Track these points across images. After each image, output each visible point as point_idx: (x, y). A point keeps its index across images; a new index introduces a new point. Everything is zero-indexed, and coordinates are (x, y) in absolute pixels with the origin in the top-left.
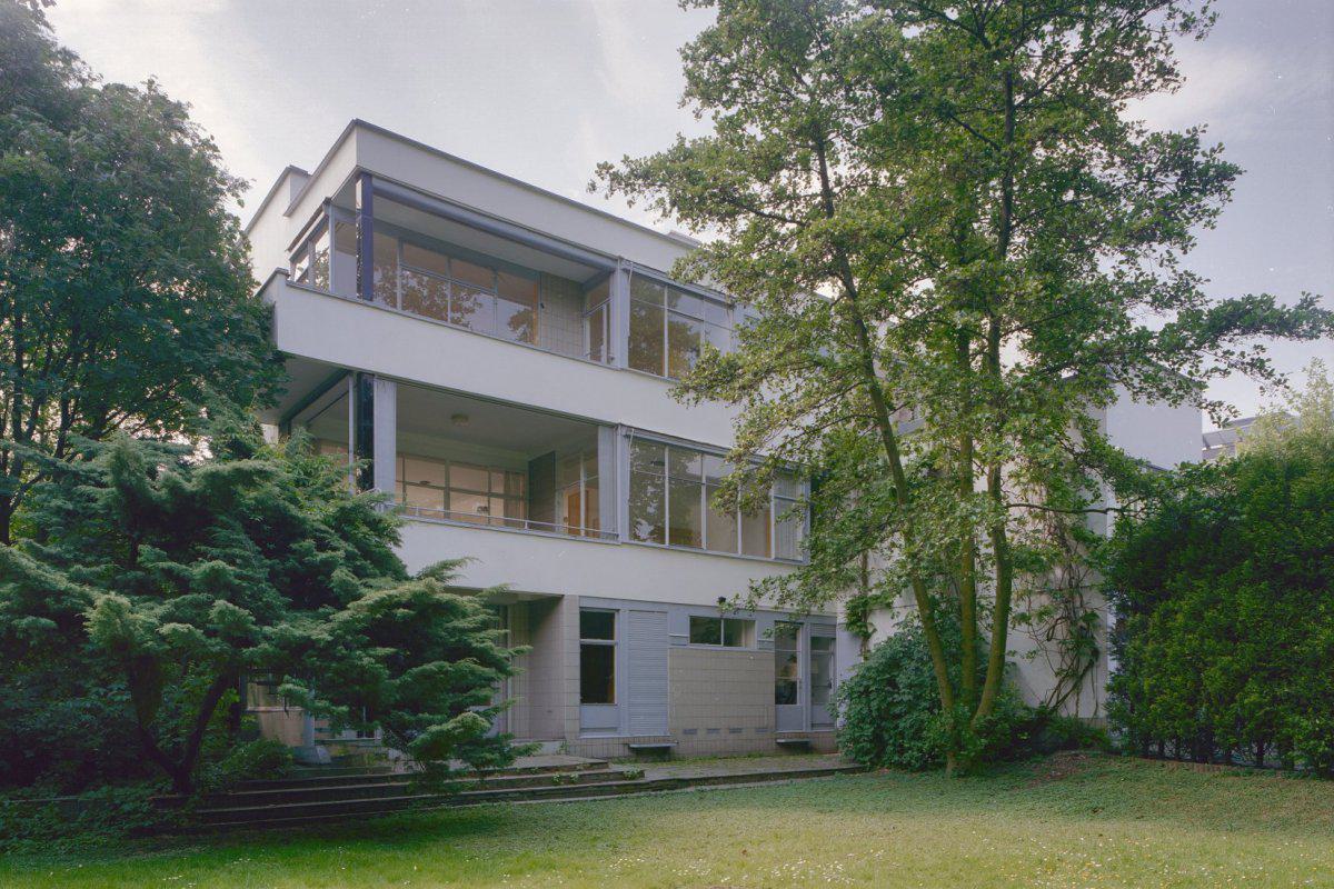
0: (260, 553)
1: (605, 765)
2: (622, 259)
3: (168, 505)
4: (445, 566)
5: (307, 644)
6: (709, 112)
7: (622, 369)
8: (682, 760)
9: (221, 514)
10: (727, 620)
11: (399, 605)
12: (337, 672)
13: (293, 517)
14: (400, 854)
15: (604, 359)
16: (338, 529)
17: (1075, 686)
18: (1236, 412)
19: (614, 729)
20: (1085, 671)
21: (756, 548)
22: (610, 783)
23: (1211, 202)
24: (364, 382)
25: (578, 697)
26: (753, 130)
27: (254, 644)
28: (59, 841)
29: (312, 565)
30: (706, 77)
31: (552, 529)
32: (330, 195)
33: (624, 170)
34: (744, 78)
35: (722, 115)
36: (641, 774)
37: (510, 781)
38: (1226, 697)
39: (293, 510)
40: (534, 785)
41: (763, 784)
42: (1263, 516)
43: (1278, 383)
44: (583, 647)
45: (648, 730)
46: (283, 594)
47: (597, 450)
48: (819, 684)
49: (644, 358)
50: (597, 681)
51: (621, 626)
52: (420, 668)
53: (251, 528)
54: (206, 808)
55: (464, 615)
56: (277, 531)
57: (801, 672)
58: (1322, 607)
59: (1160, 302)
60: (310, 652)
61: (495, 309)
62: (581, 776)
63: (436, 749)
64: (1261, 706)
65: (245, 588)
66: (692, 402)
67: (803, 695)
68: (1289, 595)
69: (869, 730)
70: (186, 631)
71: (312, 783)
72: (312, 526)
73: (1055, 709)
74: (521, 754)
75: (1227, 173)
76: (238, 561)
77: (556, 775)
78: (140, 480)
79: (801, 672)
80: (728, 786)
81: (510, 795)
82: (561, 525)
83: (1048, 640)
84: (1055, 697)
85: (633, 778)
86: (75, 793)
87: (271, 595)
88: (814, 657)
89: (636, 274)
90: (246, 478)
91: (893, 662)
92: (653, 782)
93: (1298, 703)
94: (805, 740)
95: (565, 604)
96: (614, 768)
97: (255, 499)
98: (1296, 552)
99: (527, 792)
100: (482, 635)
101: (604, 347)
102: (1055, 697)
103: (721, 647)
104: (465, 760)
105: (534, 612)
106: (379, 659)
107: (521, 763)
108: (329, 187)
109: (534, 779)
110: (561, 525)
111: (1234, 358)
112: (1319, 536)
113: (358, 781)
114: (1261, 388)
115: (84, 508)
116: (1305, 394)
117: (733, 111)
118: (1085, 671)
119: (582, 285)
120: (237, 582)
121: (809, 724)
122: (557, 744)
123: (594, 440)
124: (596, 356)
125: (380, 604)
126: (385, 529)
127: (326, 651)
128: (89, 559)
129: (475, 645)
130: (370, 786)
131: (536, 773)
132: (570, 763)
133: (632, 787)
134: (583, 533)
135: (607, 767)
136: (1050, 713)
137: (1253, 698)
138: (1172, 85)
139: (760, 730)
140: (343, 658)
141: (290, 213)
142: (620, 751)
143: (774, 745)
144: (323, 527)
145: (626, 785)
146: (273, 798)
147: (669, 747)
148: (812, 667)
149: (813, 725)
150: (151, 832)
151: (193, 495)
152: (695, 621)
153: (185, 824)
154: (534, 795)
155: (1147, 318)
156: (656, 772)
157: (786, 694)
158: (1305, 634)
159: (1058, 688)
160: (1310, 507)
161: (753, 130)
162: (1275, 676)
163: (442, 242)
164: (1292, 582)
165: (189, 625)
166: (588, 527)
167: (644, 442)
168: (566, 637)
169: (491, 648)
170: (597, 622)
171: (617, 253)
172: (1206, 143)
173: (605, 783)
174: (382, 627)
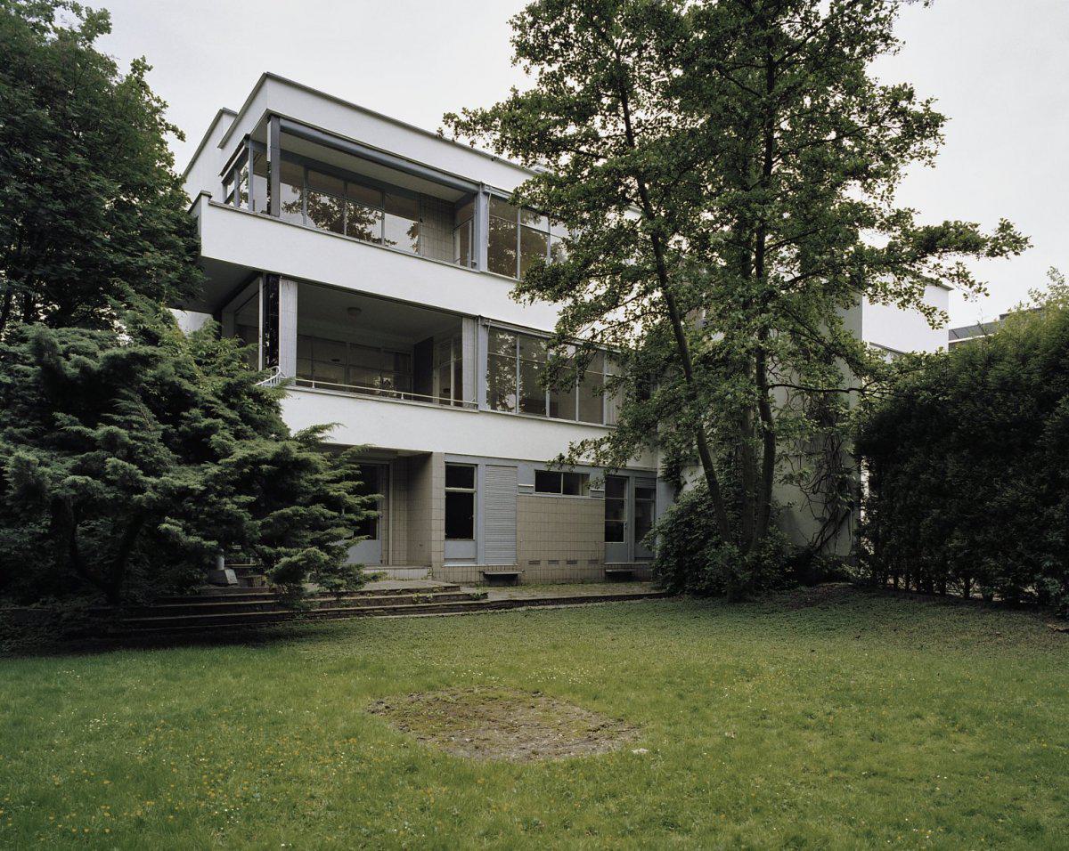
0: (155, 419)
1: (457, 588)
3: (79, 382)
4: (316, 429)
5: (185, 492)
6: (536, 69)
8: (527, 584)
9: (123, 388)
11: (266, 462)
12: (209, 515)
13: (188, 391)
15: (469, 264)
16: (224, 400)
18: (947, 317)
19: (473, 560)
21: (592, 415)
22: (458, 603)
26: (571, 82)
27: (142, 491)
28: (7, 642)
29: (198, 430)
30: (532, 42)
31: (430, 401)
33: (464, 119)
34: (563, 41)
35: (546, 71)
36: (485, 595)
37: (377, 600)
39: (187, 385)
42: (965, 396)
43: (979, 291)
44: (448, 494)
45: (500, 562)
46: (175, 451)
47: (461, 336)
48: (642, 525)
49: (499, 264)
50: (460, 522)
51: (480, 477)
52: (280, 512)
53: (147, 399)
54: (132, 617)
57: (628, 517)
59: (887, 226)
60: (188, 498)
61: (396, 227)
63: (292, 574)
65: (140, 447)
66: (528, 302)
67: (628, 533)
70: (84, 482)
72: (203, 398)
73: (820, 548)
75: (936, 120)
77: (415, 595)
78: (58, 362)
79: (628, 517)
81: (376, 611)
83: (814, 493)
84: (819, 540)
87: (163, 452)
88: (638, 504)
90: (146, 361)
91: (693, 506)
92: (492, 602)
94: (631, 570)
95: (434, 459)
96: (465, 590)
97: (154, 376)
99: (390, 609)
100: (339, 486)
101: (469, 254)
102: (819, 540)
103: (560, 495)
104: (321, 585)
106: (241, 506)
111: (943, 271)
112: (1007, 414)
113: (256, 598)
114: (965, 295)
117: (555, 67)
119: (453, 204)
120: (132, 442)
121: (633, 558)
124: (464, 263)
125: (243, 462)
127: (200, 498)
128: (22, 422)
129: (332, 493)
130: (265, 602)
131: (400, 593)
132: (428, 586)
133: (476, 605)
134: (452, 403)
135: (459, 590)
138: (893, 48)
139: (592, 562)
140: (214, 503)
141: (223, 145)
142: (477, 577)
143: (603, 574)
144: (212, 399)
145: (472, 604)
146: (186, 611)
147: (517, 575)
152: (539, 474)
154: (395, 611)
155: (873, 239)
156: (496, 594)
159: (822, 532)
160: (1000, 390)
161: (571, 82)
166: (453, 397)
167: (495, 329)
168: (436, 486)
169: (344, 497)
170: (460, 474)
171: (478, 179)
173: (454, 603)
174: (249, 477)
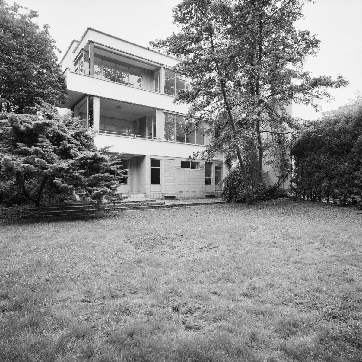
2: (163, 64)
5: (62, 169)
6: (181, 25)
7: (163, 94)
10: (192, 162)
12: (70, 177)
14: (32, 226)
16: (75, 138)
17: (283, 181)
20: (286, 176)
23: (315, 49)
24: (91, 97)
25: (150, 182)
27: (47, 169)
29: (66, 148)
31: (145, 137)
32: (83, 48)
33: (156, 43)
35: (184, 26)
36: (164, 203)
37: (127, 205)
38: (318, 183)
40: (134, 206)
41: (198, 206)
42: (327, 135)
44: (151, 169)
45: (170, 192)
47: (156, 117)
48: (218, 179)
50: (155, 178)
52: (94, 175)
53: (48, 138)
55: (107, 162)
56: (57, 139)
57: (213, 176)
58: (343, 160)
61: (133, 79)
62: (147, 204)
63: (98, 197)
64: (326, 186)
65: (46, 154)
66: (179, 104)
67: (213, 182)
68: (335, 157)
69: (228, 192)
71: (73, 205)
73: (278, 186)
74: (124, 198)
76: (44, 147)
79: (213, 176)
80: (187, 207)
82: (147, 136)
84: (278, 183)
85: (162, 204)
86: (8, 208)
87: (54, 155)
88: (216, 172)
89: (166, 68)
91: (235, 173)
93: (337, 186)
96: (157, 201)
97: (51, 130)
98: (336, 145)
101: (158, 88)
103: (190, 169)
104: (108, 200)
105: (138, 160)
106: (81, 173)
107: (124, 200)
108: (83, 45)
109: (134, 204)
110: (147, 136)
115: (6, 132)
116: (355, 100)
117: (187, 25)
118: (286, 176)
122: (144, 195)
123: (155, 113)
125: (81, 159)
126: (89, 138)
127: (67, 171)
129: (112, 169)
131: (135, 203)
133: (161, 206)
134: (153, 138)
136: (277, 187)
137: (324, 184)
140: (72, 173)
141: (74, 52)
142: (162, 197)
146: (62, 209)
147: (175, 196)
148: (216, 174)
149: (216, 190)
150: (27, 218)
151: (32, 129)
153: (37, 216)
155: (296, 82)
156: (168, 203)
157: (208, 182)
158: (338, 167)
159: (279, 181)
161: (193, 30)
162: (331, 178)
163: (115, 60)
164: (335, 153)
165: (28, 164)
168: (147, 167)
170: (155, 162)
171: (161, 63)
172: (311, 34)
174: (83, 164)
